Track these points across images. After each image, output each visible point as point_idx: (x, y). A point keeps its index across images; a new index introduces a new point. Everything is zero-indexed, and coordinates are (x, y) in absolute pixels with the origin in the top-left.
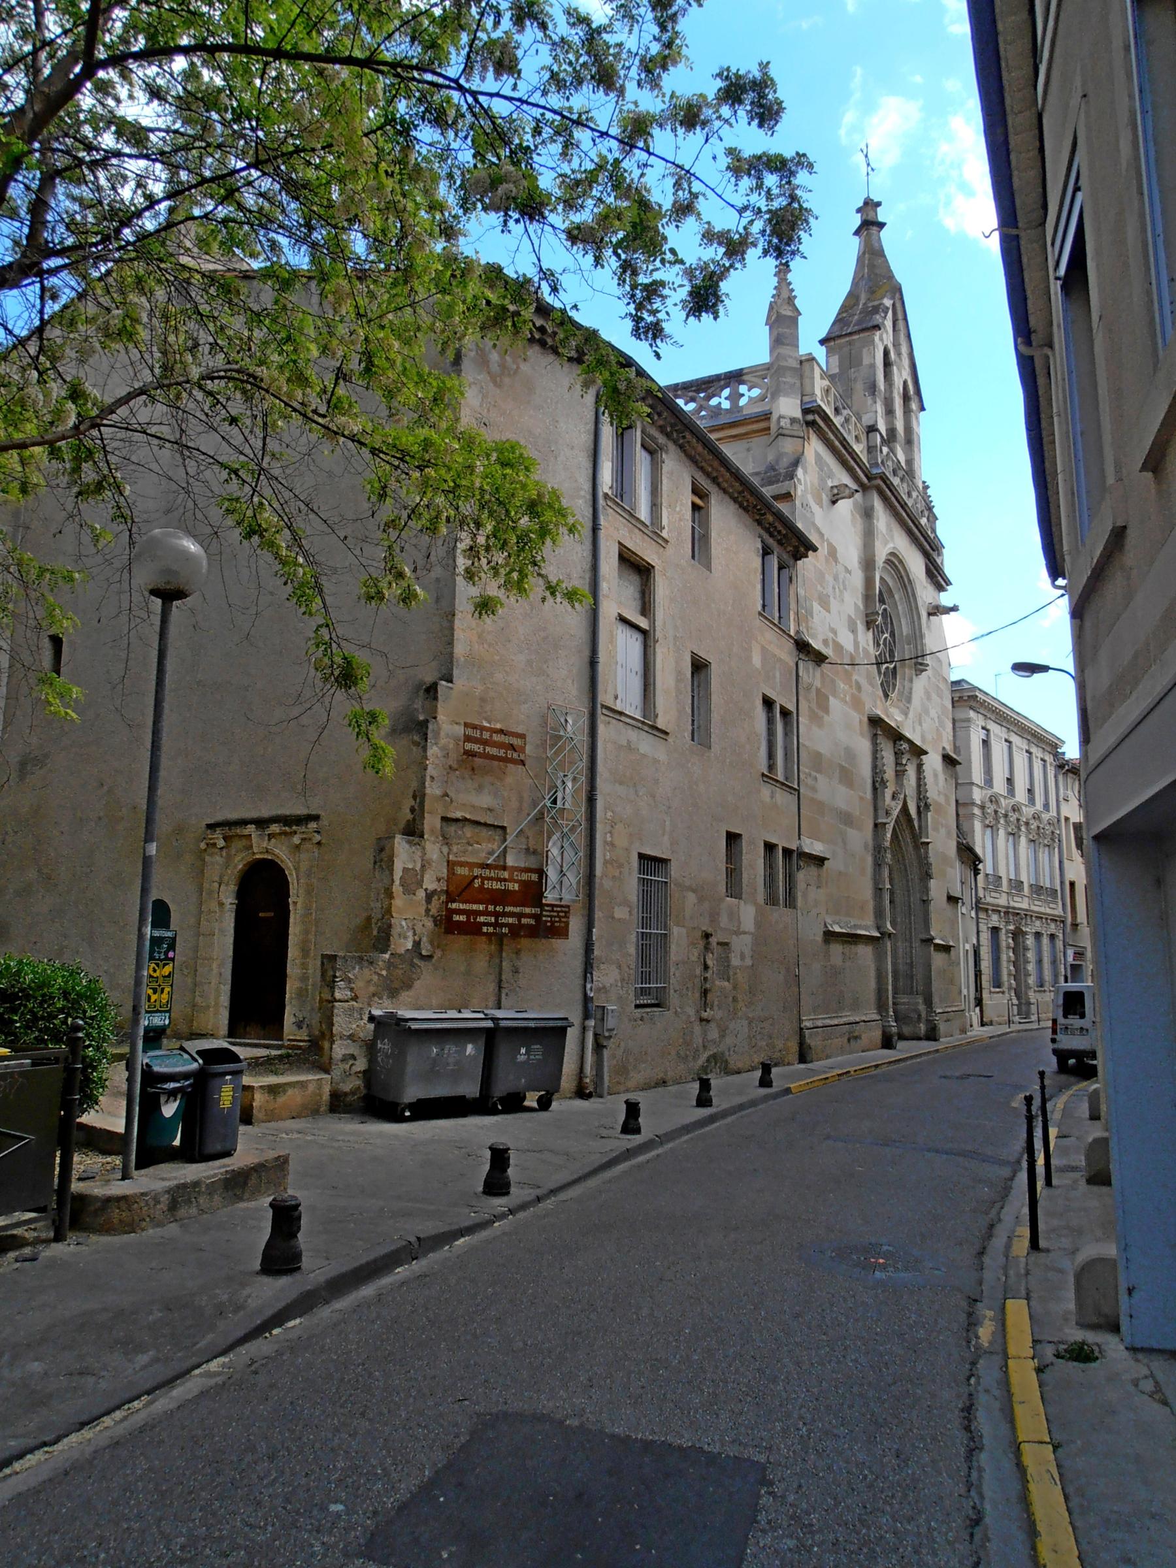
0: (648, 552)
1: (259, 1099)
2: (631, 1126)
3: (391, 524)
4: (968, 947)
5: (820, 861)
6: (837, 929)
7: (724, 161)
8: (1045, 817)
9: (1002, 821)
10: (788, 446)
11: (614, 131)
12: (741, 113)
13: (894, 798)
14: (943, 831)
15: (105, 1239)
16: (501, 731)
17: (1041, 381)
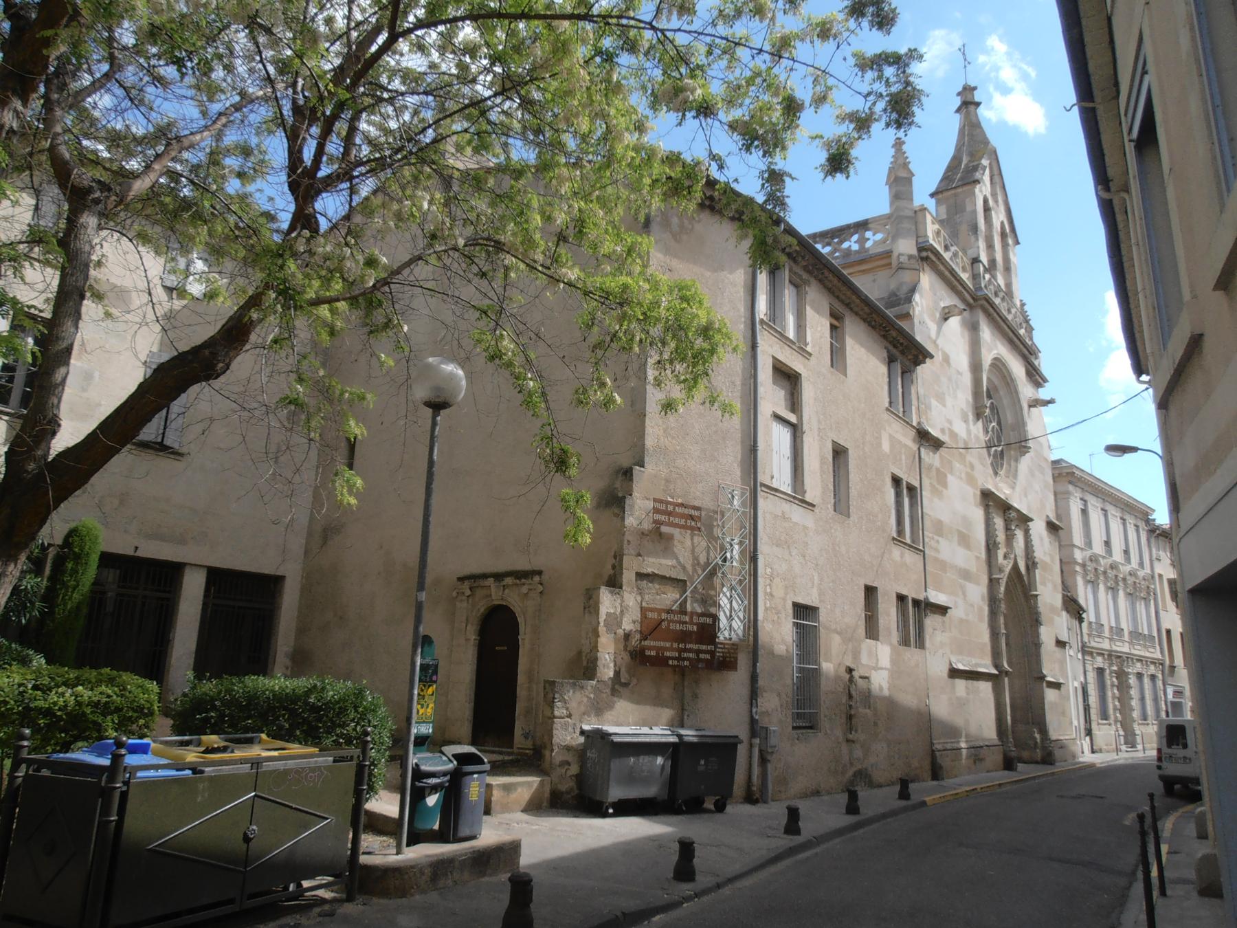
0: (795, 363)
1: (496, 795)
2: (792, 826)
3: (598, 346)
4: (1076, 684)
5: (943, 610)
6: (961, 667)
7: (852, 61)
8: (1141, 574)
10: (907, 277)
11: (767, 47)
12: (865, 23)
13: (1005, 557)
14: (1050, 585)
15: (383, 901)
16: (682, 505)
17: (1119, 218)
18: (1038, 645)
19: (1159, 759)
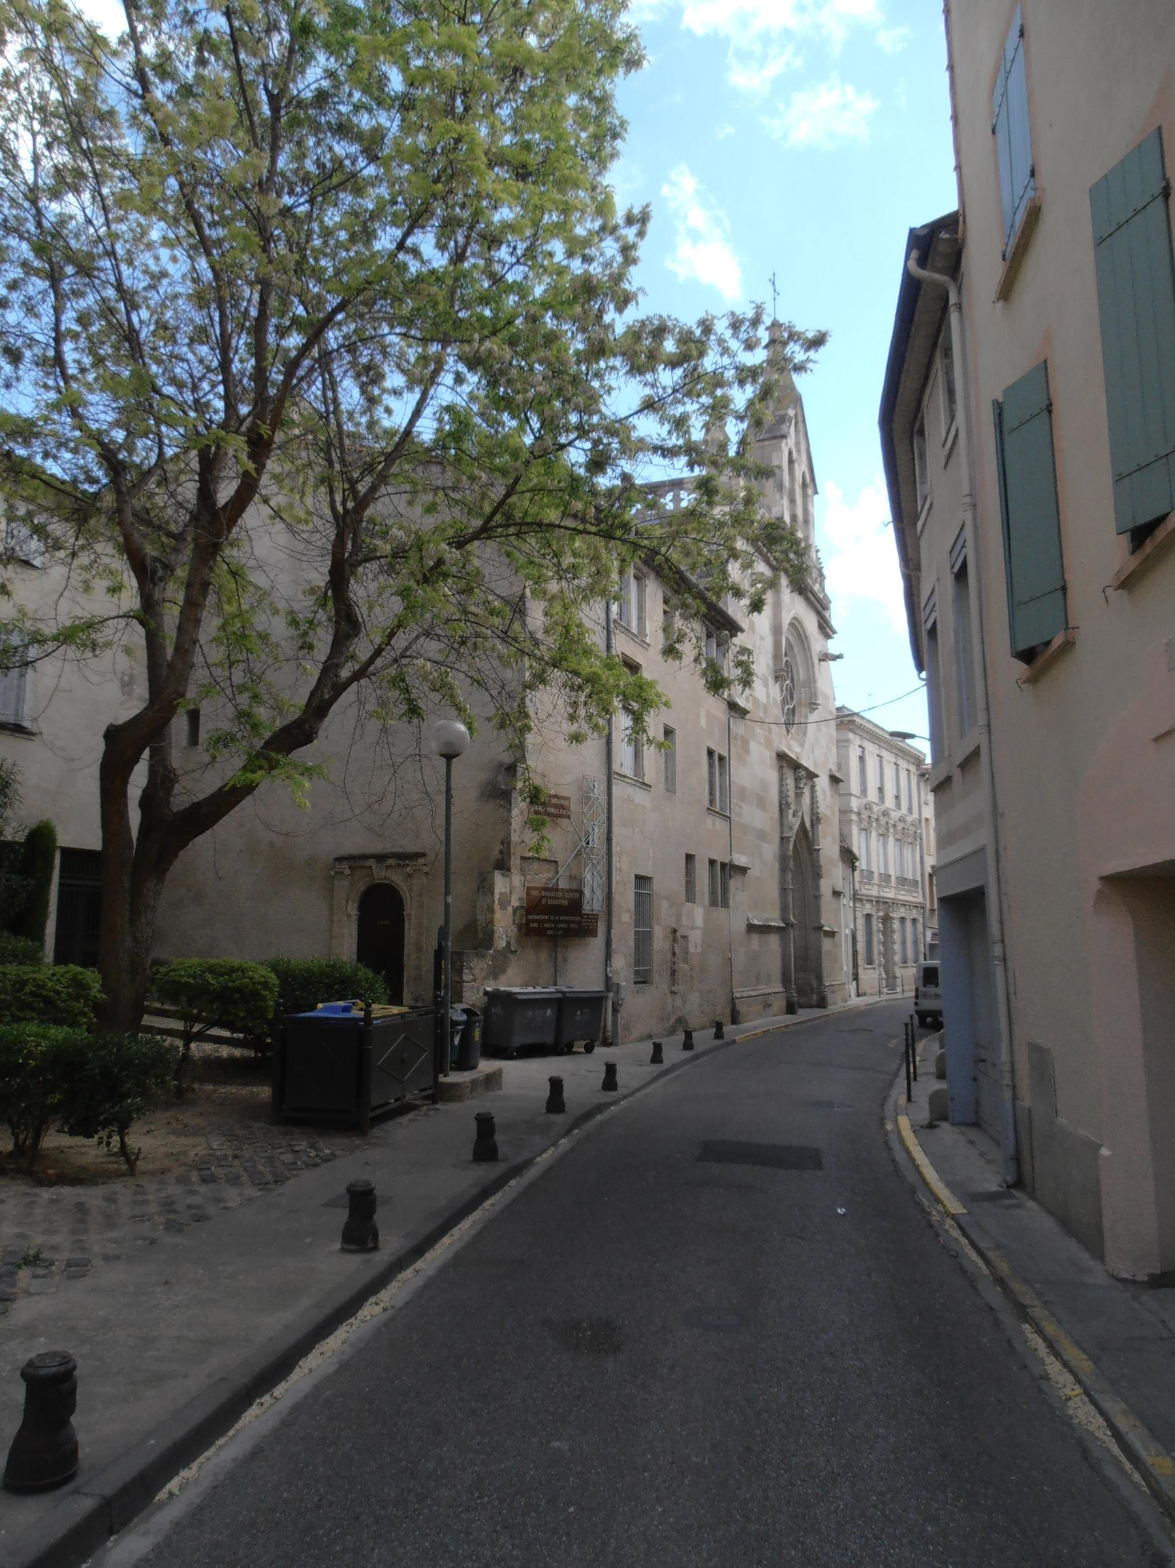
4: (847, 931)
5: (743, 870)
6: (756, 922)
8: (909, 819)
9: (874, 824)
13: (794, 815)
18: (817, 897)
19: (917, 997)
